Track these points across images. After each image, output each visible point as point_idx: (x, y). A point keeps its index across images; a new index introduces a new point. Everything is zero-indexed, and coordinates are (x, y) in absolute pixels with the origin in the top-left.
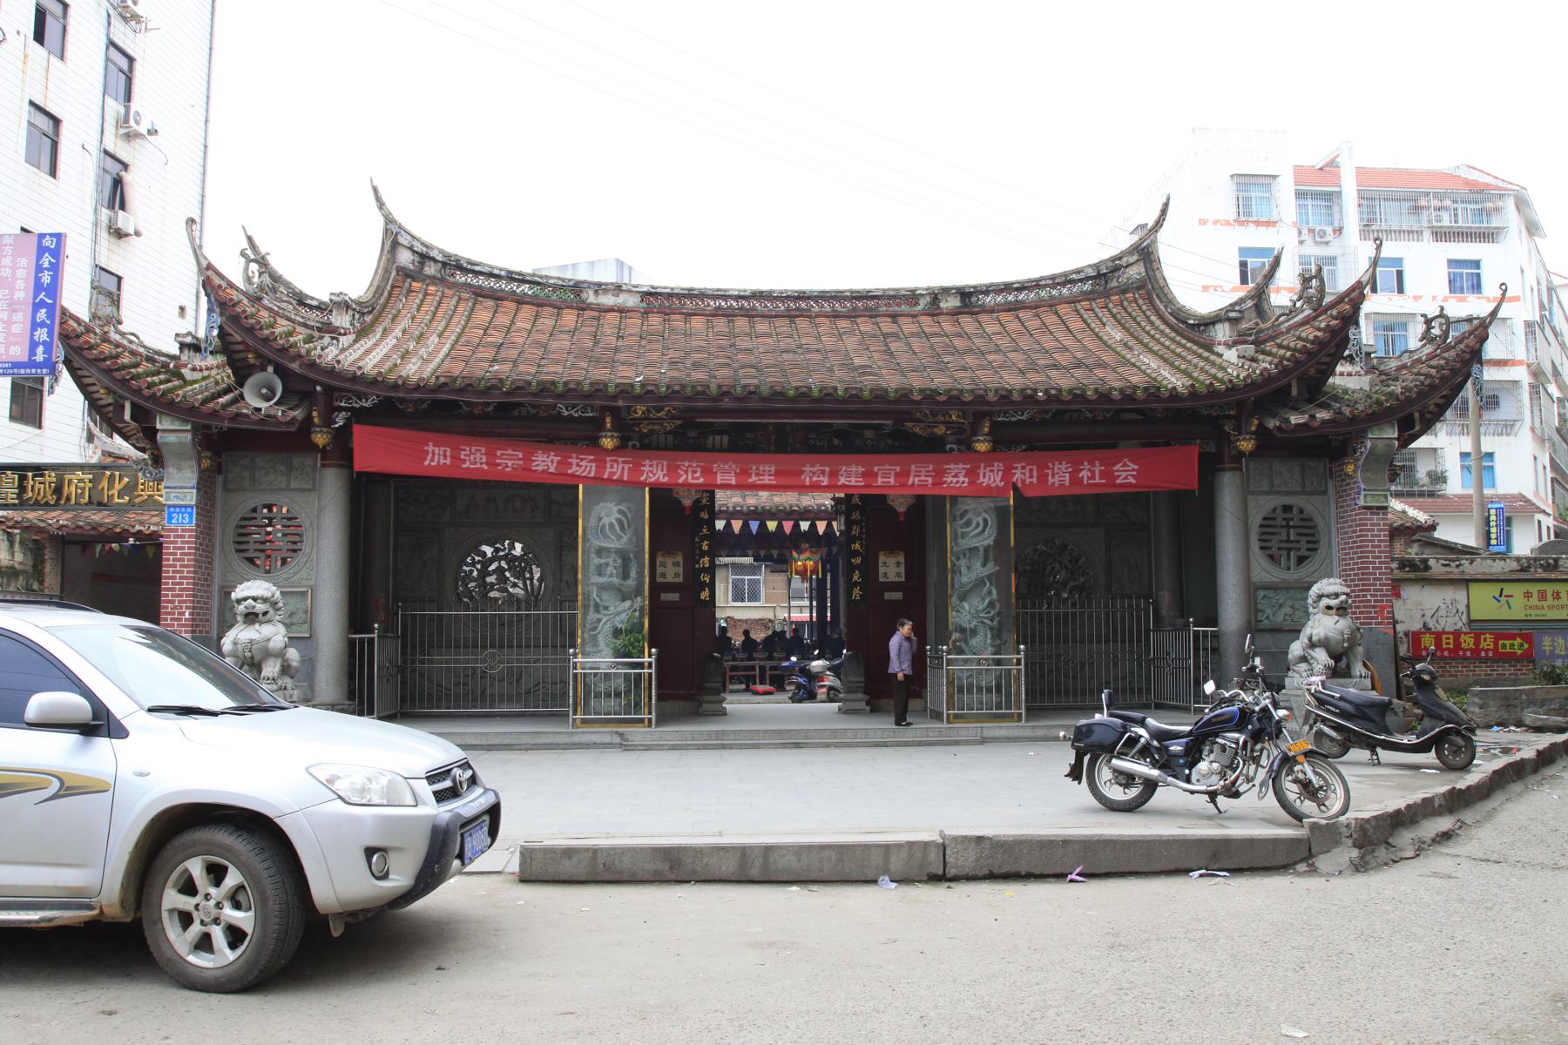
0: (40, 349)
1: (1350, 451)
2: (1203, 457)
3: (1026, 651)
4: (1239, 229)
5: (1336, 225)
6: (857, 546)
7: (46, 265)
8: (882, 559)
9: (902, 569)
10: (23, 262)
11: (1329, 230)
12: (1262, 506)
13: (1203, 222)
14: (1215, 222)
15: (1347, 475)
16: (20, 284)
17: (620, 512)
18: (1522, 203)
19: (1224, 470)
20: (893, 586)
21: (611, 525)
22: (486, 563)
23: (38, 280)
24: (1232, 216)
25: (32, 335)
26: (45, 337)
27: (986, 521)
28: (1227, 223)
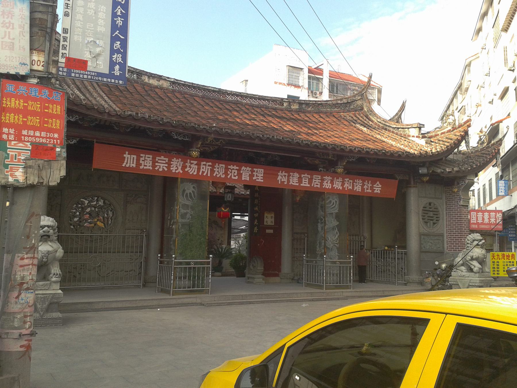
0: (117, 67)
1: (456, 183)
2: (400, 182)
3: (353, 258)
4: (289, 88)
5: (320, 90)
6: (256, 209)
7: (119, 13)
8: (266, 215)
9: (273, 220)
10: (103, 8)
11: (318, 93)
12: (424, 202)
13: (276, 83)
14: (280, 83)
15: (454, 192)
16: (101, 22)
17: (194, 187)
18: (380, 91)
19: (410, 187)
20: (270, 227)
21: (190, 193)
22: (83, 209)
23: (113, 22)
24: (286, 82)
25: (111, 58)
26: (120, 60)
27: (336, 201)
28: (284, 84)
